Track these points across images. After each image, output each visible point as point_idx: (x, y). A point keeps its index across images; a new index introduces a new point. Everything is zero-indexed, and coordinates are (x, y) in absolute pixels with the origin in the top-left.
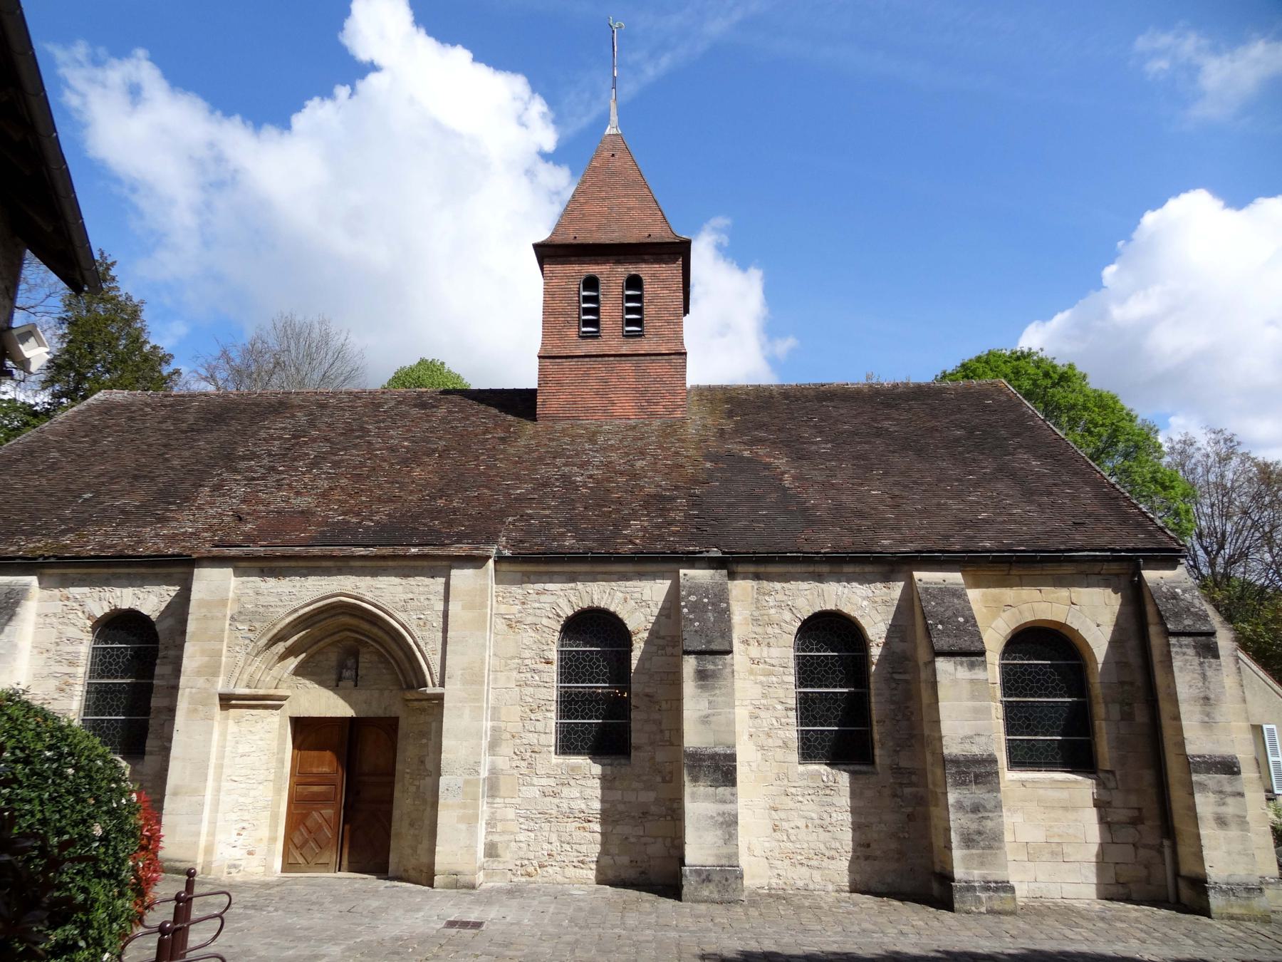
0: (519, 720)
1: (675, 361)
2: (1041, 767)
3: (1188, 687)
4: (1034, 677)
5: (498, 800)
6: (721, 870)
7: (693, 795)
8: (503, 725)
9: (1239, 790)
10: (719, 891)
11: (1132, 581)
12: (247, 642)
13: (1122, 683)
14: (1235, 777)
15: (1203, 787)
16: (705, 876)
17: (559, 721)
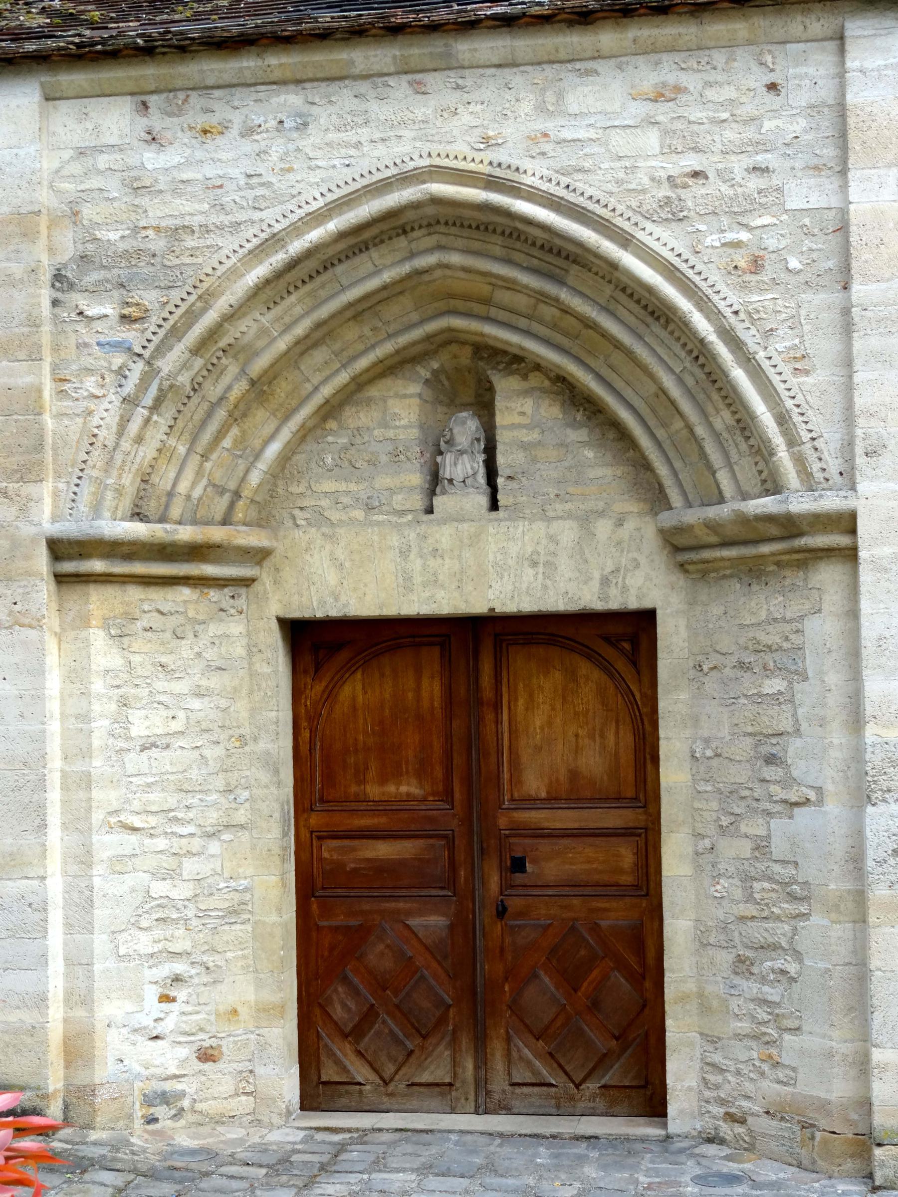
12: (118, 360)
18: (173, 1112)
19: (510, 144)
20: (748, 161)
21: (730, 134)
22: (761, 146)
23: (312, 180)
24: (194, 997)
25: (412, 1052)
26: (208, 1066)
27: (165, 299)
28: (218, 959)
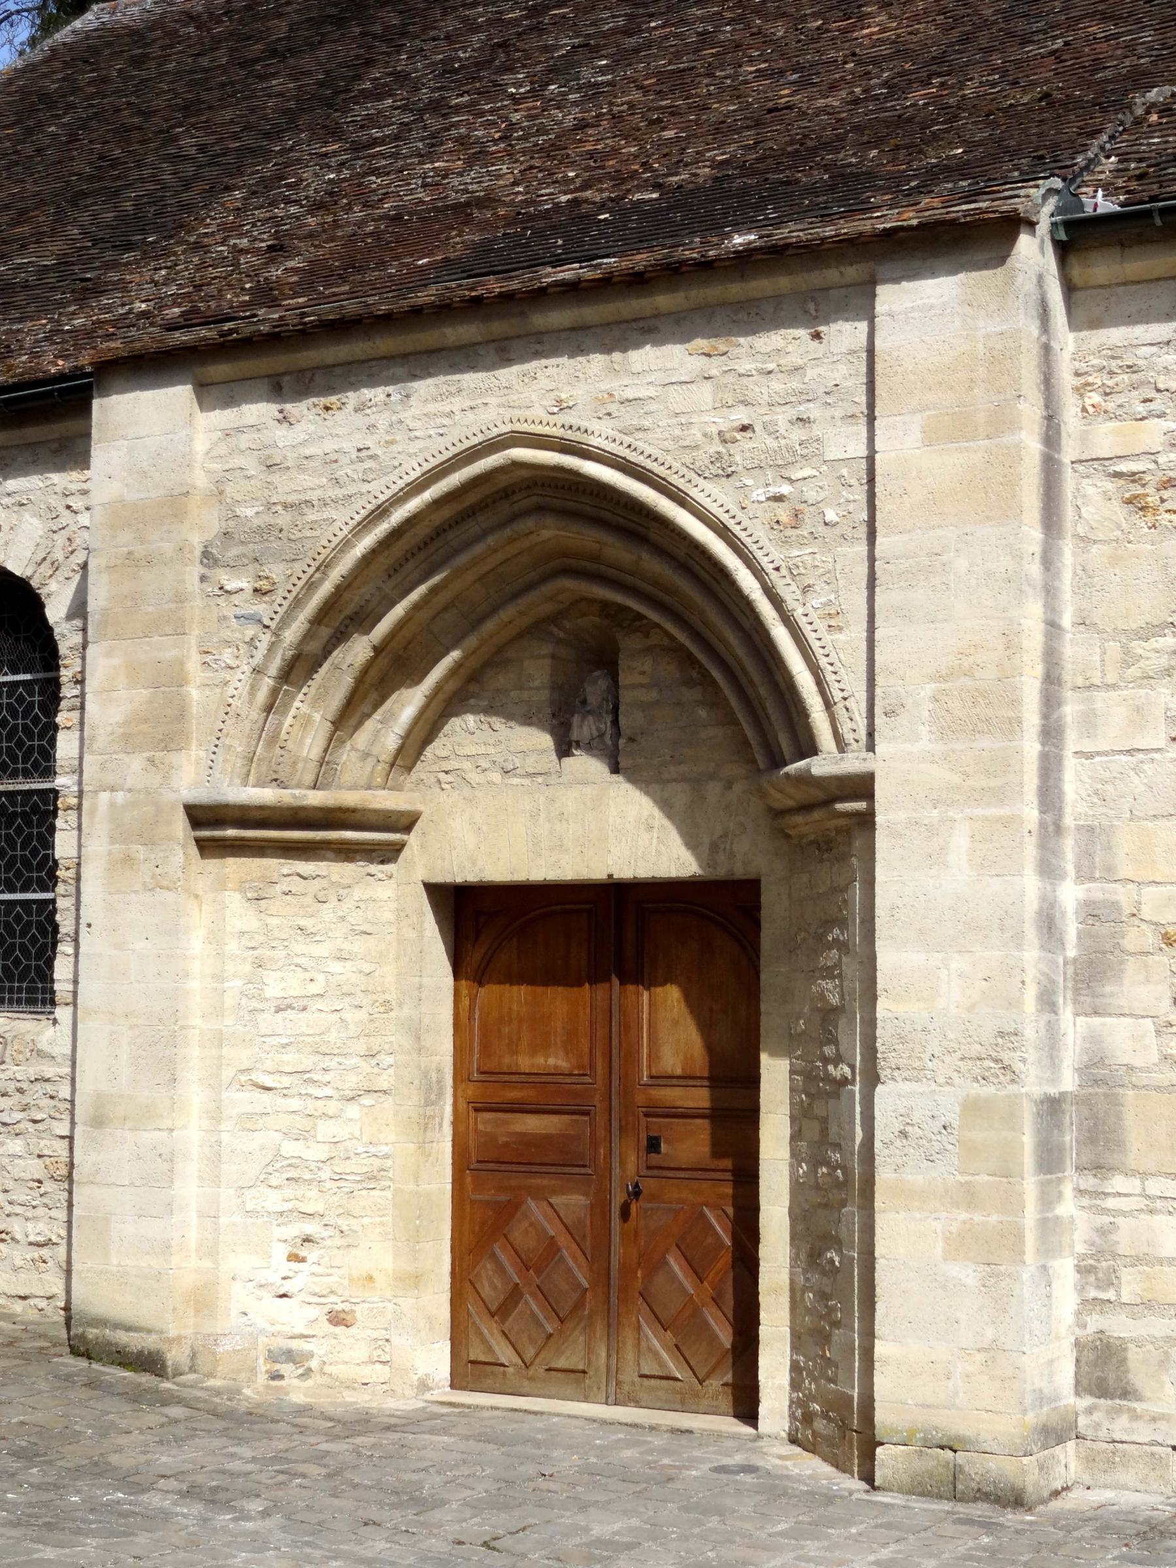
5: (1119, 1183)
8: (1123, 895)
12: (251, 631)
18: (301, 1371)
19: (580, 407)
20: (792, 413)
21: (777, 385)
23: (411, 451)
24: (326, 1259)
25: (551, 1335)
26: (340, 1330)
27: (289, 572)
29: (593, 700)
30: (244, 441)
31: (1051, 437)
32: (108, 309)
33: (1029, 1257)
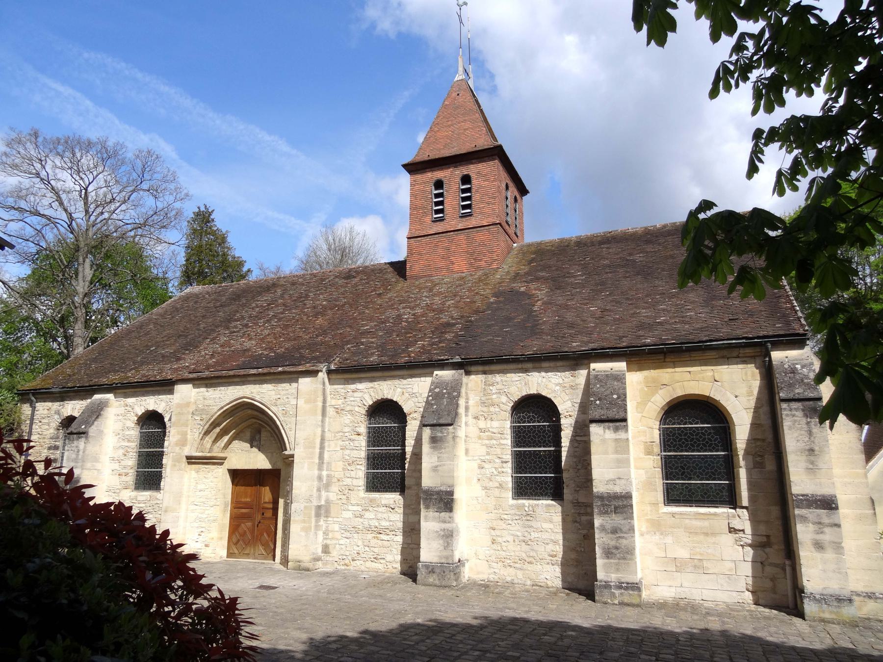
0: (341, 470)
1: (492, 229)
2: (693, 503)
3: (795, 442)
4: (689, 437)
6: (440, 566)
7: (426, 517)
8: (332, 473)
9: (836, 522)
10: (439, 579)
11: (764, 362)
12: (199, 426)
13: (756, 440)
14: (833, 511)
15: (804, 519)
16: (431, 569)
17: (514, 475)
20: (286, 396)
22: (288, 394)
28: (211, 529)
29: (257, 439)
30: (200, 394)
31: (324, 401)
32: (181, 364)
33: (312, 531)
